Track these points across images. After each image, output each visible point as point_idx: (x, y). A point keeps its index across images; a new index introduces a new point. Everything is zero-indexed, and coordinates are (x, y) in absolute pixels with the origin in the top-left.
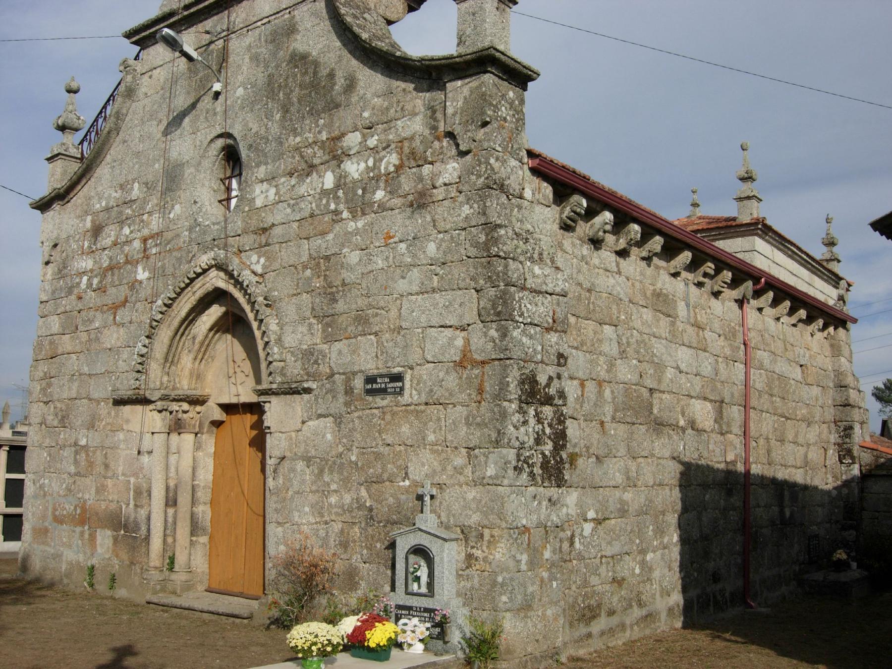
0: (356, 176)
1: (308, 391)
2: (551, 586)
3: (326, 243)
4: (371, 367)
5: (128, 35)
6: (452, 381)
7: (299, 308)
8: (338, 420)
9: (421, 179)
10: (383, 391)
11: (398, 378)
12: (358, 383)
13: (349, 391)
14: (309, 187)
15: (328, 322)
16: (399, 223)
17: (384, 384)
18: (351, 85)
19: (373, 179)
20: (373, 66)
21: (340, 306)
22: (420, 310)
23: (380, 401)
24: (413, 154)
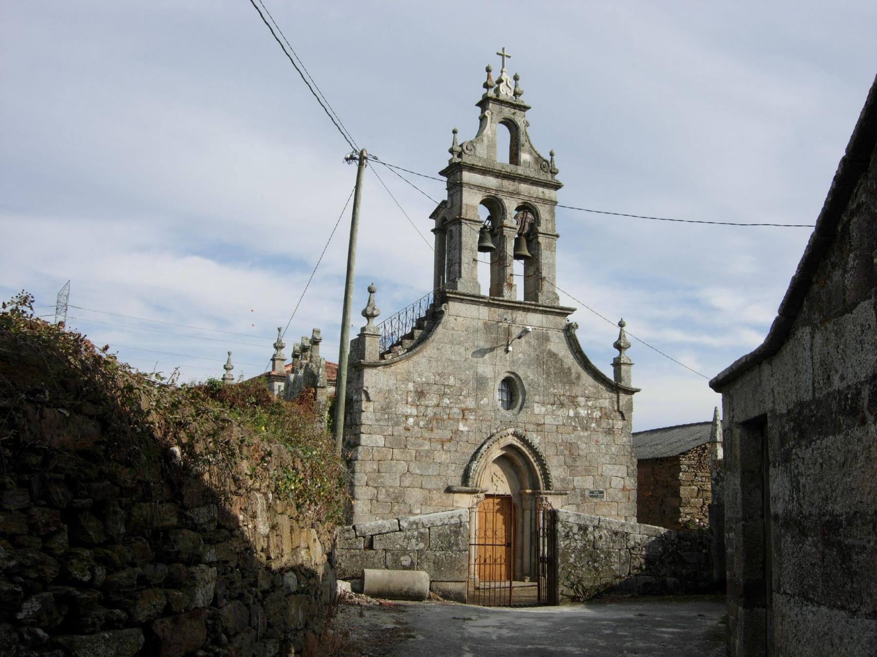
0: (141, 618)
1: (566, 494)
2: (42, 381)
3: (572, 438)
4: (591, 488)
5: (431, 217)
6: (620, 495)
7: (558, 461)
8: (578, 506)
9: (608, 424)
10: (596, 497)
11: (602, 492)
12: (587, 493)
13: (583, 496)
14: (562, 412)
15: (572, 469)
16: (602, 439)
17: (596, 494)
18: (578, 377)
19: (590, 418)
20: (589, 373)
21: (578, 463)
22: (608, 470)
23: (595, 500)
24: (606, 414)
